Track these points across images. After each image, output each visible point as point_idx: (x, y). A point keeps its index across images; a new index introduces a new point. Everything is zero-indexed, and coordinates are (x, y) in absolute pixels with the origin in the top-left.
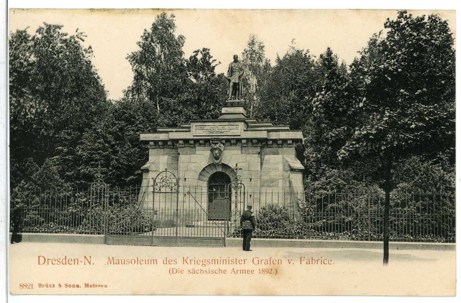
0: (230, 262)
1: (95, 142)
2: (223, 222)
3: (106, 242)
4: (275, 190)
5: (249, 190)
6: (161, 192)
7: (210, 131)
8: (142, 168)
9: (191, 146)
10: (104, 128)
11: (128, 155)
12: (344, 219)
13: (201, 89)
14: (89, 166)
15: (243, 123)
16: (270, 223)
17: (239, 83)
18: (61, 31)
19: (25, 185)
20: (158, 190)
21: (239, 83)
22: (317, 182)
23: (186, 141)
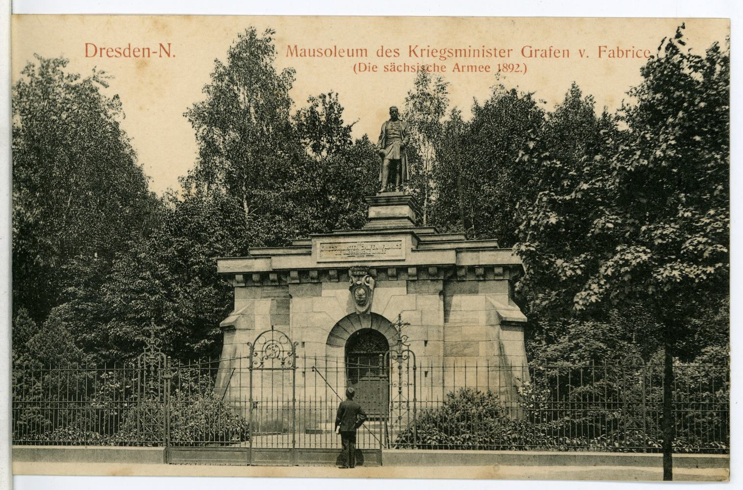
0: (486, 54)
1: (135, 276)
2: (378, 423)
3: (167, 458)
4: (471, 362)
5: (422, 362)
6: (264, 367)
7: (347, 252)
8: (221, 324)
9: (313, 281)
10: (150, 250)
11: (196, 301)
12: (604, 416)
13: (327, 172)
14: (124, 321)
15: (409, 237)
16: (463, 424)
17: (400, 160)
18: (66, 71)
19: (17, 359)
20: (259, 364)
21: (400, 160)
22: (553, 347)
23: (303, 273)
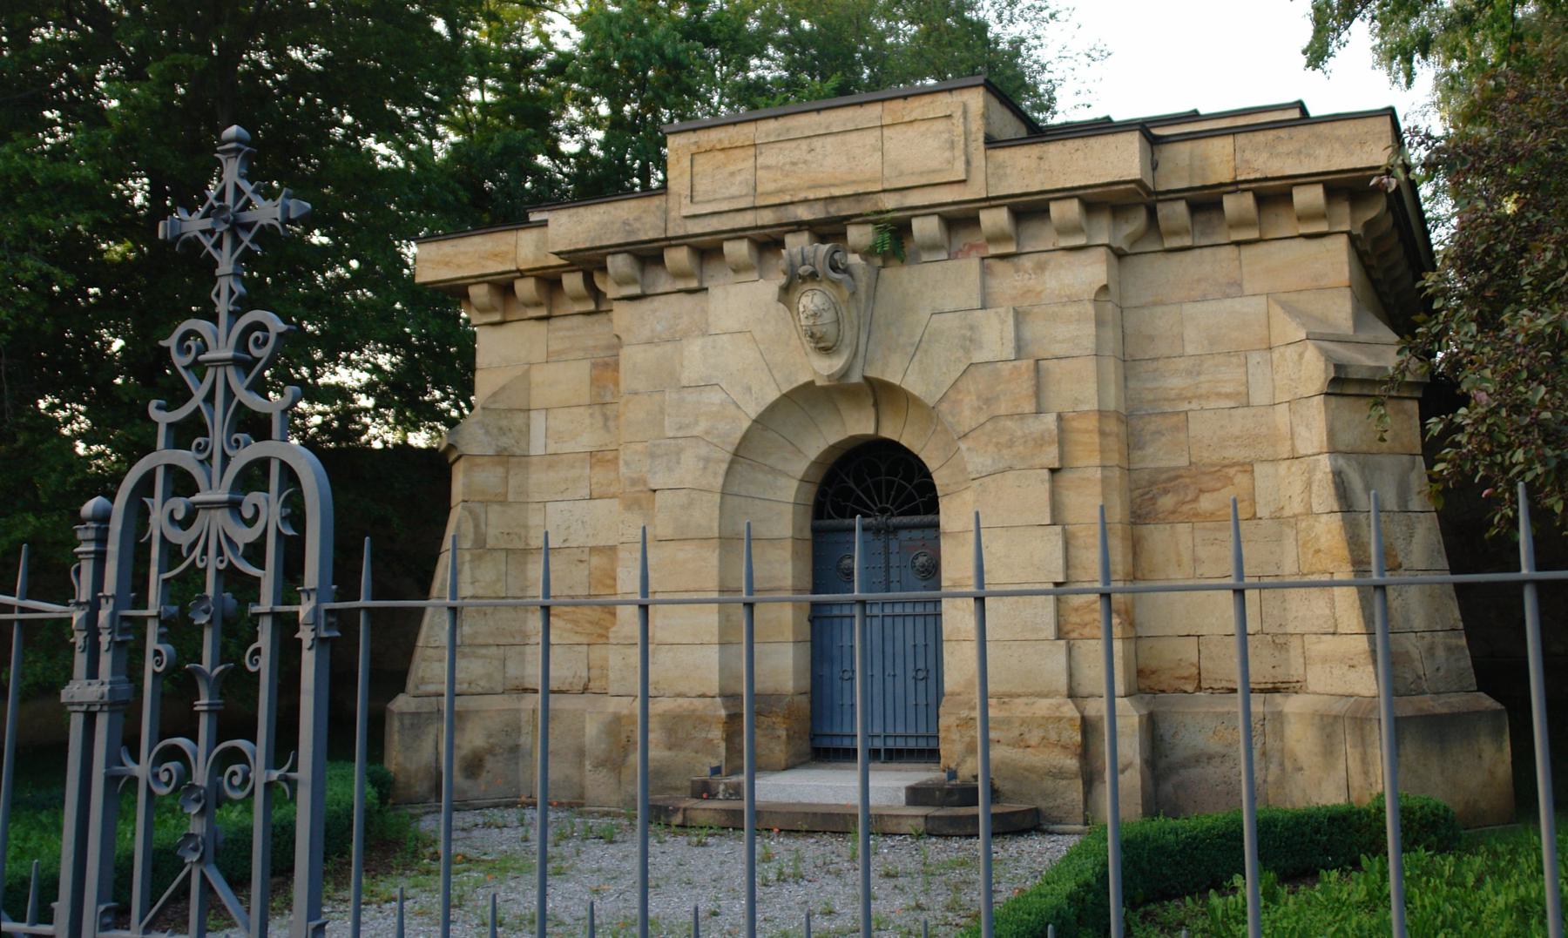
23: (648, 255)
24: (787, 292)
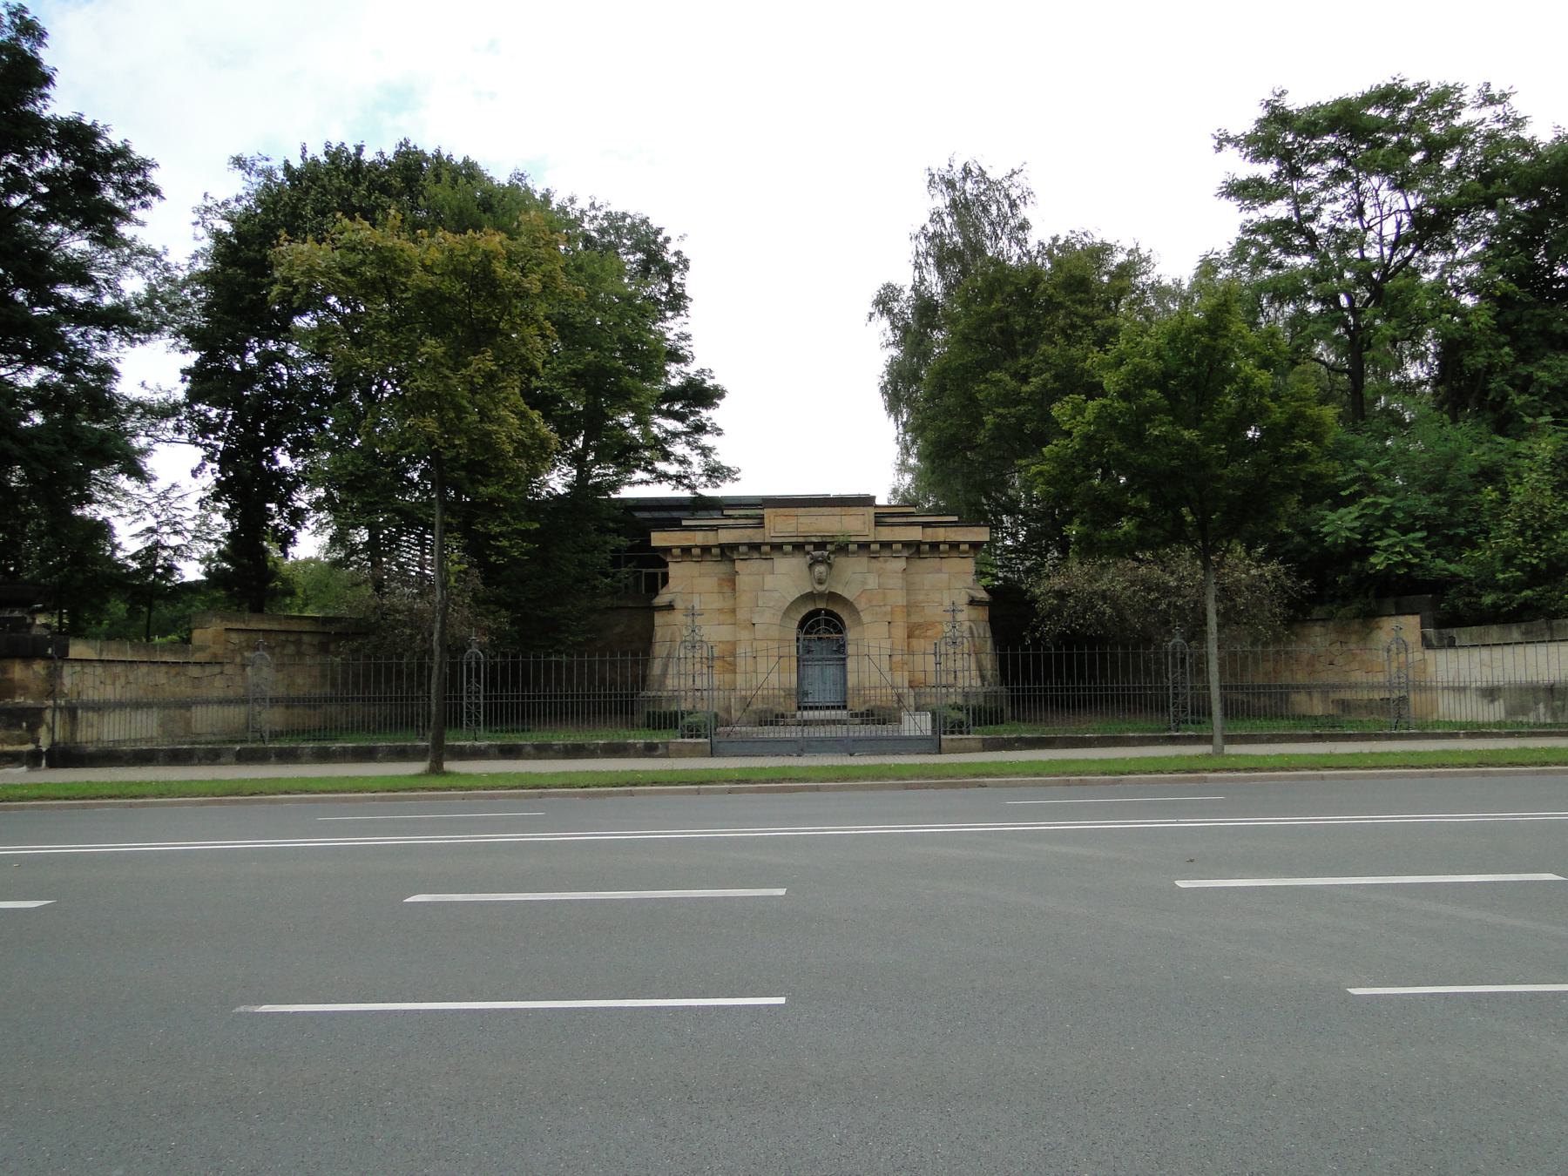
23: (755, 547)
24: (120, 543)
